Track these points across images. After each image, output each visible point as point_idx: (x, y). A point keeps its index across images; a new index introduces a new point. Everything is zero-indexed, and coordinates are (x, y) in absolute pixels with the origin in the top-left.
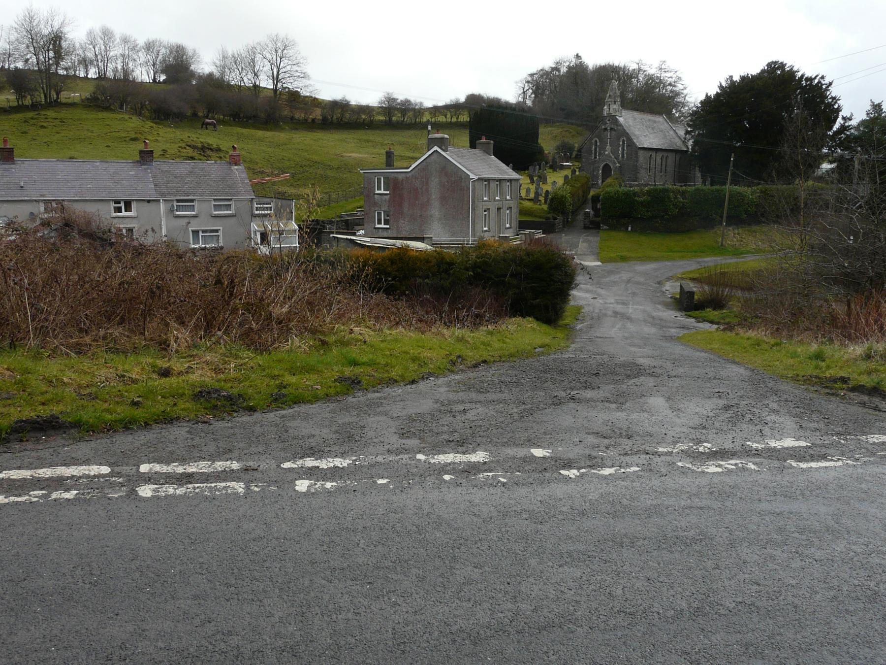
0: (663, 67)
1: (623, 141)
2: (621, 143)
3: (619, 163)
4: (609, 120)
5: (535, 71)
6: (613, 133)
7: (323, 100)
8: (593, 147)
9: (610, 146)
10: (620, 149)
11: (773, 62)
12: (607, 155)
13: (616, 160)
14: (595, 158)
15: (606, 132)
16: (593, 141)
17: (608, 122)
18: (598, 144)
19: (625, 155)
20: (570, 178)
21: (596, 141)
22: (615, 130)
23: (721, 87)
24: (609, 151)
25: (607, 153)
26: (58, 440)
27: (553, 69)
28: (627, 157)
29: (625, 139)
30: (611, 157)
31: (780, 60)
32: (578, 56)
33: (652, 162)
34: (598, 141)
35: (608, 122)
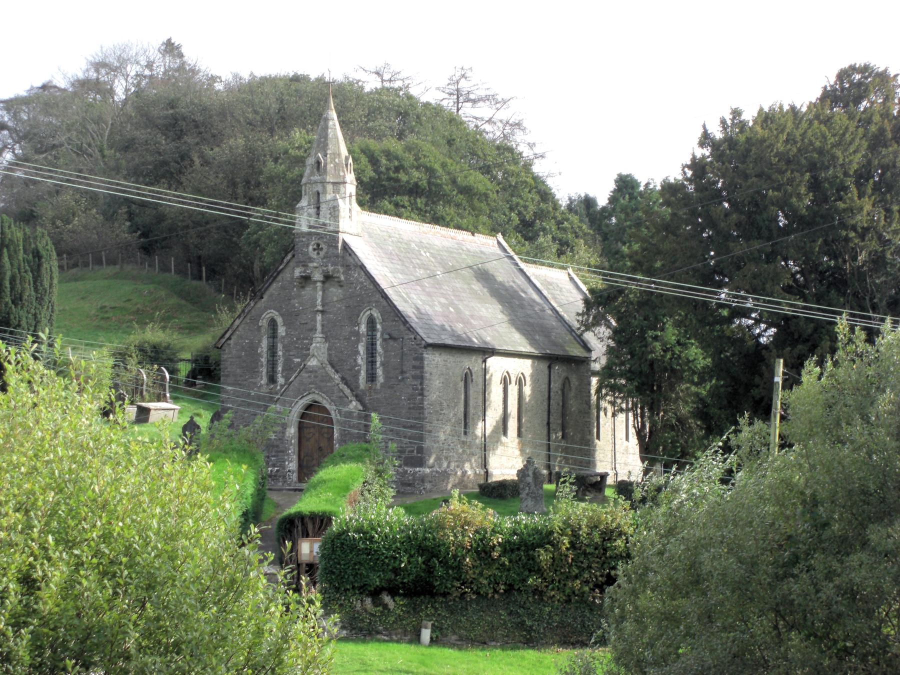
0: (464, 85)
1: (371, 322)
2: (363, 328)
3: (359, 398)
4: (318, 248)
5: (22, 92)
6: (335, 292)
7: (398, 642)
8: (265, 344)
9: (326, 339)
10: (362, 348)
11: (853, 69)
12: (313, 371)
13: (347, 391)
14: (272, 379)
15: (308, 290)
16: (264, 323)
17: (314, 255)
18: (282, 331)
19: (380, 372)
20: (204, 432)
21: (273, 323)
22: (340, 284)
23: (706, 139)
24: (324, 358)
25: (313, 363)
26: (454, 352)
27: (84, 85)
28: (387, 377)
29: (376, 314)
30: (331, 379)
31: (879, 64)
32: (170, 48)
33: (471, 392)
34: (279, 320)
35: (314, 255)
